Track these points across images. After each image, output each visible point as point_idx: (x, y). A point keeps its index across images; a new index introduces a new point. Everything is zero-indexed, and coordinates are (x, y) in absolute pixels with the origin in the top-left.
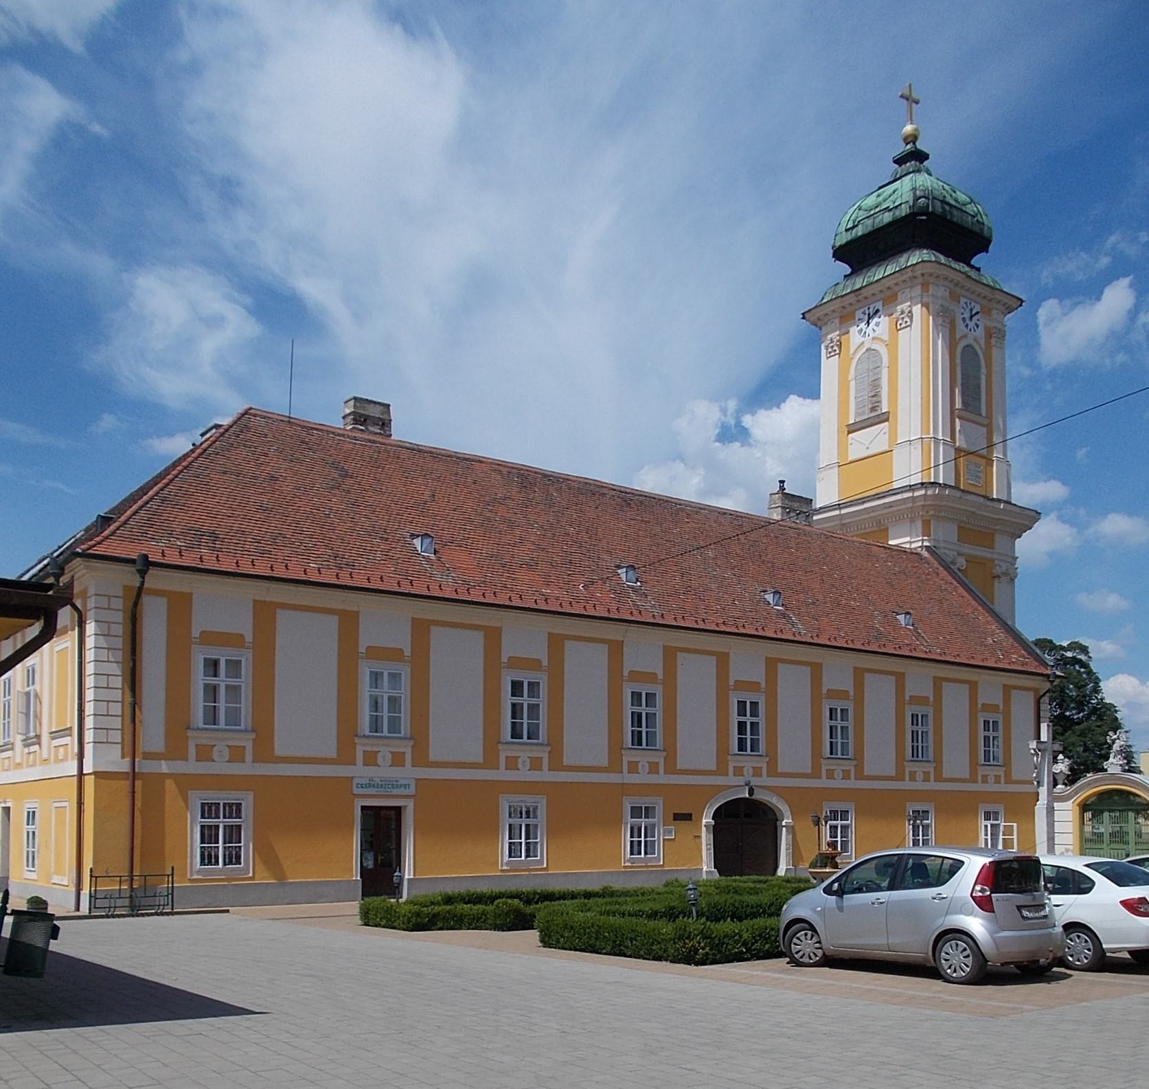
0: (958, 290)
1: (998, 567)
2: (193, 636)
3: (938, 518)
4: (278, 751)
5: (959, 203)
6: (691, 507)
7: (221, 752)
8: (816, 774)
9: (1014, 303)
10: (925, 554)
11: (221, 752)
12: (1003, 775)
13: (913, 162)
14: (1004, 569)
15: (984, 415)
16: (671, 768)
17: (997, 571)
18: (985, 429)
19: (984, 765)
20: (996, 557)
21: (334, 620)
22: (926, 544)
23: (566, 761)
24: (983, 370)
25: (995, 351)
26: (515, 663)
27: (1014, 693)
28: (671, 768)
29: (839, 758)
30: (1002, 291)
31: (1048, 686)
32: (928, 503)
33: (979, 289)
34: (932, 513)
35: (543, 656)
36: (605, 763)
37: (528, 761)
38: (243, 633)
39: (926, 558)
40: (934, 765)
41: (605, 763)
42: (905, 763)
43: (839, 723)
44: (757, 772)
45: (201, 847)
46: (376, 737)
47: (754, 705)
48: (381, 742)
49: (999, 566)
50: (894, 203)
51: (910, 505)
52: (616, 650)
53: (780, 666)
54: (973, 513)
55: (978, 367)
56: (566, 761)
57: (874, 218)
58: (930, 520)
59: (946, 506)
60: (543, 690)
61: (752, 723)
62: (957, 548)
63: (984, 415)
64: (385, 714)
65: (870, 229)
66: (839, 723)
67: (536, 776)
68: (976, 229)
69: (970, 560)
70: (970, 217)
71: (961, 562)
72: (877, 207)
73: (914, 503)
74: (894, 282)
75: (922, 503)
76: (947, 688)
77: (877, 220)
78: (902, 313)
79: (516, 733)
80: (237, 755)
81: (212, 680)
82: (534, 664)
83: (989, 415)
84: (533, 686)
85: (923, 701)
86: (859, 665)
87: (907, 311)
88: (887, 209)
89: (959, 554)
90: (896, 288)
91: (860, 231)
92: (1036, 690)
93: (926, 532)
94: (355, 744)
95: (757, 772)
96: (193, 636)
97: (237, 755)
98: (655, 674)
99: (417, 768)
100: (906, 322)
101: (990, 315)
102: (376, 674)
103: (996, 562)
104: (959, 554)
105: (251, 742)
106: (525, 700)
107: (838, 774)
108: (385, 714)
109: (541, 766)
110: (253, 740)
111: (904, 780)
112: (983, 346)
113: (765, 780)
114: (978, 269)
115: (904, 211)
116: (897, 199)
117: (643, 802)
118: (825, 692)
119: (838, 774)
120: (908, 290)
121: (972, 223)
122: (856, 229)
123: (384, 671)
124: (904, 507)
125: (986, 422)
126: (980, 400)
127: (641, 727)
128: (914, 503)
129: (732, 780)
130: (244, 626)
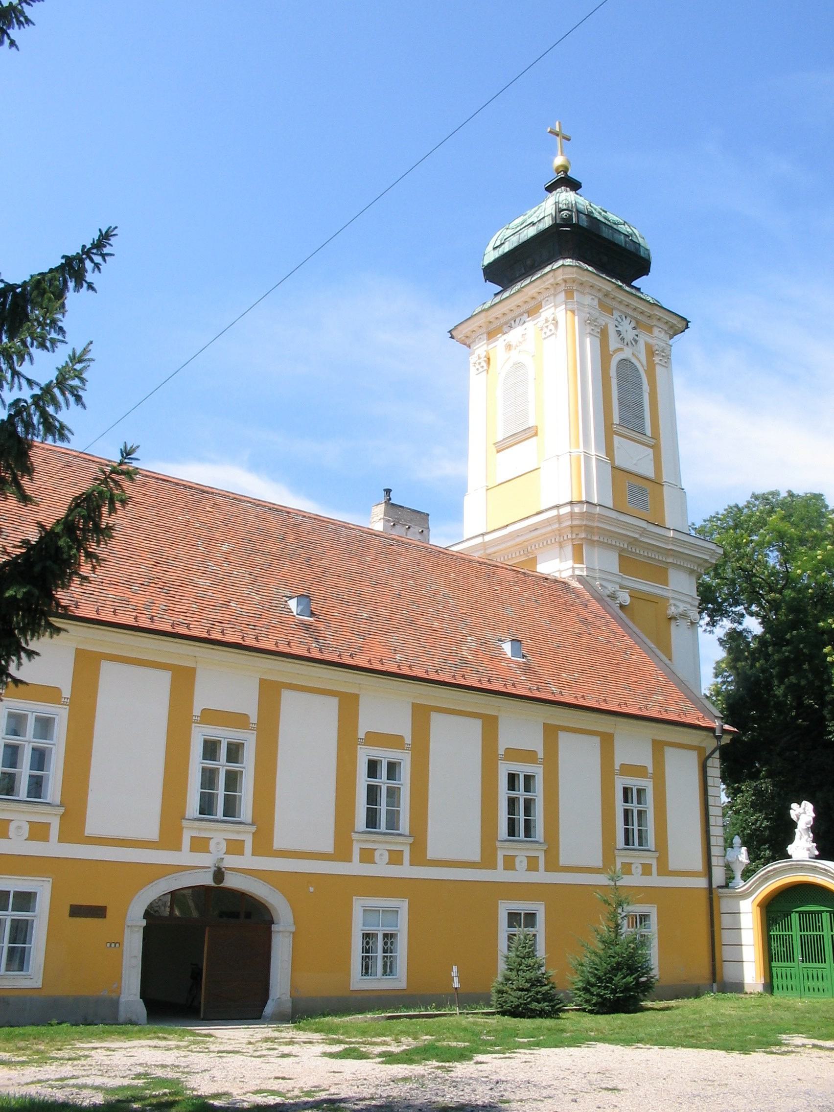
0: (608, 301)
1: (673, 608)
2: (539, 757)
3: (592, 542)
4: (91, 829)
5: (609, 221)
6: (333, 524)
7: (382, 856)
8: (342, 853)
9: (681, 325)
10: (575, 584)
11: (382, 856)
12: (654, 863)
13: (563, 188)
14: (681, 610)
15: (649, 433)
16: (553, 865)
17: (672, 611)
18: (650, 451)
19: (506, 841)
20: (670, 594)
21: (334, 702)
22: (578, 572)
23: (431, 854)
24: (646, 387)
25: (659, 370)
26: (374, 739)
27: (563, 737)
28: (553, 865)
29: (217, 821)
30: (661, 307)
31: (714, 743)
32: (576, 523)
33: (634, 303)
34: (583, 535)
35: (540, 750)
36: (477, 858)
37: (26, 827)
38: (403, 735)
39: (574, 588)
40: (657, 854)
41: (477, 858)
42: (616, 852)
43: (521, 794)
44: (235, 847)
45: (384, 957)
46: (514, 841)
47: (528, 779)
48: (212, 824)
49: (675, 605)
50: (538, 218)
51: (556, 526)
52: (490, 725)
53: (435, 717)
54: (636, 539)
55: (639, 385)
56: (431, 854)
57: (519, 234)
58: (582, 544)
59: (597, 527)
60: (539, 784)
61: (389, 789)
62: (619, 580)
63: (649, 433)
64: (221, 792)
65: (515, 244)
66: (634, 806)
67: (36, 849)
68: (632, 249)
69: (635, 595)
70: (622, 237)
71: (625, 597)
72: (522, 224)
73: (560, 523)
74: (537, 290)
75: (569, 523)
76: (671, 754)
77: (522, 236)
78: (547, 321)
79: (512, 831)
80: (395, 858)
81: (210, 764)
82: (395, 741)
83: (656, 436)
84: (393, 768)
85: (638, 771)
86: (658, 738)
87: (550, 319)
88: (533, 224)
89: (622, 587)
90: (540, 298)
91: (506, 248)
92: (699, 749)
93: (578, 557)
94: (181, 829)
95: (235, 847)
96: (539, 757)
97: (395, 858)
98: (402, 736)
99: (549, 873)
100: (551, 330)
101: (651, 333)
102: (514, 775)
103: (672, 601)
104: (622, 587)
105: (251, 836)
106: (383, 781)
107: (521, 863)
108: (221, 792)
109: (48, 836)
110: (253, 834)
111: (494, 867)
112: (645, 363)
113: (248, 860)
114: (638, 289)
115: (548, 223)
116: (540, 213)
117: (522, 906)
118: (617, 767)
119: (521, 863)
120: (552, 298)
121: (626, 242)
122: (503, 246)
123: (520, 773)
124: (549, 529)
125: (652, 442)
126: (643, 418)
127: (639, 830)
128: (560, 523)
129: (185, 857)
130: (403, 728)
